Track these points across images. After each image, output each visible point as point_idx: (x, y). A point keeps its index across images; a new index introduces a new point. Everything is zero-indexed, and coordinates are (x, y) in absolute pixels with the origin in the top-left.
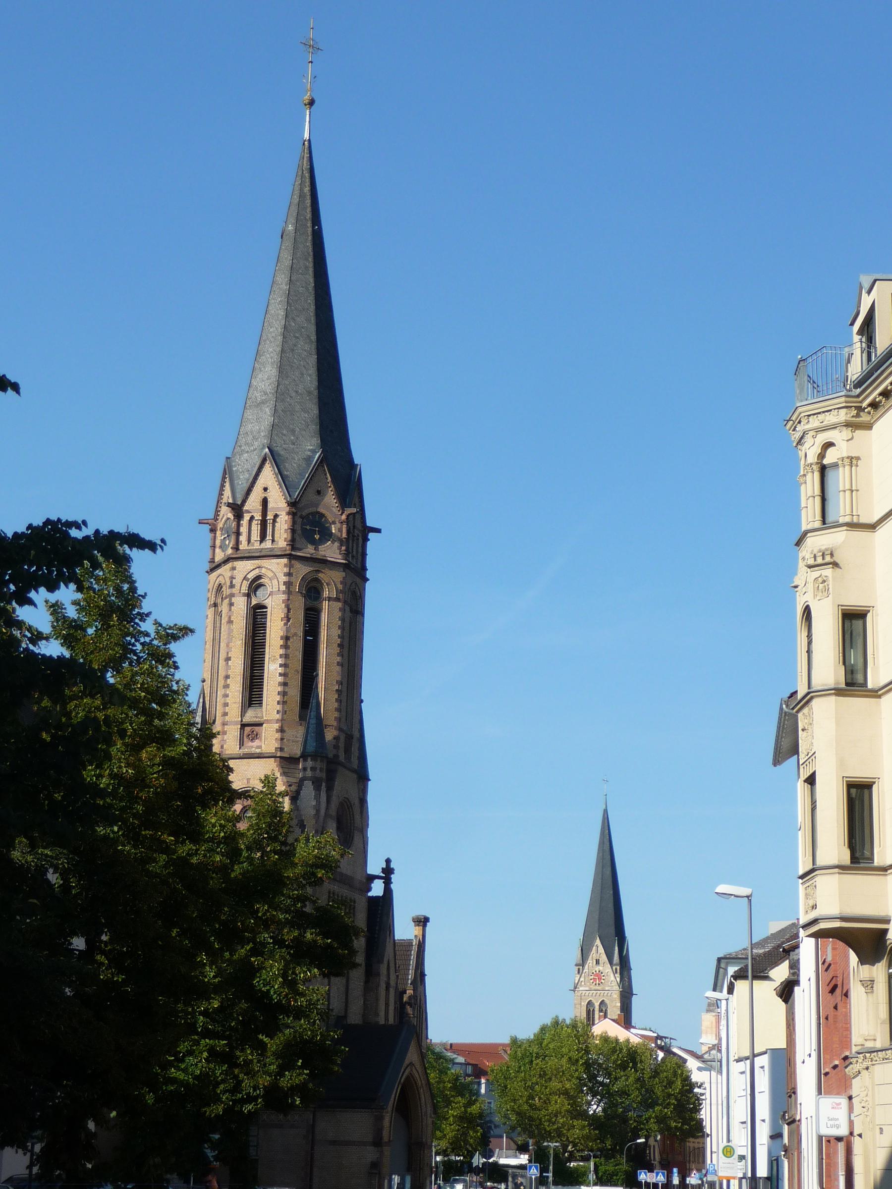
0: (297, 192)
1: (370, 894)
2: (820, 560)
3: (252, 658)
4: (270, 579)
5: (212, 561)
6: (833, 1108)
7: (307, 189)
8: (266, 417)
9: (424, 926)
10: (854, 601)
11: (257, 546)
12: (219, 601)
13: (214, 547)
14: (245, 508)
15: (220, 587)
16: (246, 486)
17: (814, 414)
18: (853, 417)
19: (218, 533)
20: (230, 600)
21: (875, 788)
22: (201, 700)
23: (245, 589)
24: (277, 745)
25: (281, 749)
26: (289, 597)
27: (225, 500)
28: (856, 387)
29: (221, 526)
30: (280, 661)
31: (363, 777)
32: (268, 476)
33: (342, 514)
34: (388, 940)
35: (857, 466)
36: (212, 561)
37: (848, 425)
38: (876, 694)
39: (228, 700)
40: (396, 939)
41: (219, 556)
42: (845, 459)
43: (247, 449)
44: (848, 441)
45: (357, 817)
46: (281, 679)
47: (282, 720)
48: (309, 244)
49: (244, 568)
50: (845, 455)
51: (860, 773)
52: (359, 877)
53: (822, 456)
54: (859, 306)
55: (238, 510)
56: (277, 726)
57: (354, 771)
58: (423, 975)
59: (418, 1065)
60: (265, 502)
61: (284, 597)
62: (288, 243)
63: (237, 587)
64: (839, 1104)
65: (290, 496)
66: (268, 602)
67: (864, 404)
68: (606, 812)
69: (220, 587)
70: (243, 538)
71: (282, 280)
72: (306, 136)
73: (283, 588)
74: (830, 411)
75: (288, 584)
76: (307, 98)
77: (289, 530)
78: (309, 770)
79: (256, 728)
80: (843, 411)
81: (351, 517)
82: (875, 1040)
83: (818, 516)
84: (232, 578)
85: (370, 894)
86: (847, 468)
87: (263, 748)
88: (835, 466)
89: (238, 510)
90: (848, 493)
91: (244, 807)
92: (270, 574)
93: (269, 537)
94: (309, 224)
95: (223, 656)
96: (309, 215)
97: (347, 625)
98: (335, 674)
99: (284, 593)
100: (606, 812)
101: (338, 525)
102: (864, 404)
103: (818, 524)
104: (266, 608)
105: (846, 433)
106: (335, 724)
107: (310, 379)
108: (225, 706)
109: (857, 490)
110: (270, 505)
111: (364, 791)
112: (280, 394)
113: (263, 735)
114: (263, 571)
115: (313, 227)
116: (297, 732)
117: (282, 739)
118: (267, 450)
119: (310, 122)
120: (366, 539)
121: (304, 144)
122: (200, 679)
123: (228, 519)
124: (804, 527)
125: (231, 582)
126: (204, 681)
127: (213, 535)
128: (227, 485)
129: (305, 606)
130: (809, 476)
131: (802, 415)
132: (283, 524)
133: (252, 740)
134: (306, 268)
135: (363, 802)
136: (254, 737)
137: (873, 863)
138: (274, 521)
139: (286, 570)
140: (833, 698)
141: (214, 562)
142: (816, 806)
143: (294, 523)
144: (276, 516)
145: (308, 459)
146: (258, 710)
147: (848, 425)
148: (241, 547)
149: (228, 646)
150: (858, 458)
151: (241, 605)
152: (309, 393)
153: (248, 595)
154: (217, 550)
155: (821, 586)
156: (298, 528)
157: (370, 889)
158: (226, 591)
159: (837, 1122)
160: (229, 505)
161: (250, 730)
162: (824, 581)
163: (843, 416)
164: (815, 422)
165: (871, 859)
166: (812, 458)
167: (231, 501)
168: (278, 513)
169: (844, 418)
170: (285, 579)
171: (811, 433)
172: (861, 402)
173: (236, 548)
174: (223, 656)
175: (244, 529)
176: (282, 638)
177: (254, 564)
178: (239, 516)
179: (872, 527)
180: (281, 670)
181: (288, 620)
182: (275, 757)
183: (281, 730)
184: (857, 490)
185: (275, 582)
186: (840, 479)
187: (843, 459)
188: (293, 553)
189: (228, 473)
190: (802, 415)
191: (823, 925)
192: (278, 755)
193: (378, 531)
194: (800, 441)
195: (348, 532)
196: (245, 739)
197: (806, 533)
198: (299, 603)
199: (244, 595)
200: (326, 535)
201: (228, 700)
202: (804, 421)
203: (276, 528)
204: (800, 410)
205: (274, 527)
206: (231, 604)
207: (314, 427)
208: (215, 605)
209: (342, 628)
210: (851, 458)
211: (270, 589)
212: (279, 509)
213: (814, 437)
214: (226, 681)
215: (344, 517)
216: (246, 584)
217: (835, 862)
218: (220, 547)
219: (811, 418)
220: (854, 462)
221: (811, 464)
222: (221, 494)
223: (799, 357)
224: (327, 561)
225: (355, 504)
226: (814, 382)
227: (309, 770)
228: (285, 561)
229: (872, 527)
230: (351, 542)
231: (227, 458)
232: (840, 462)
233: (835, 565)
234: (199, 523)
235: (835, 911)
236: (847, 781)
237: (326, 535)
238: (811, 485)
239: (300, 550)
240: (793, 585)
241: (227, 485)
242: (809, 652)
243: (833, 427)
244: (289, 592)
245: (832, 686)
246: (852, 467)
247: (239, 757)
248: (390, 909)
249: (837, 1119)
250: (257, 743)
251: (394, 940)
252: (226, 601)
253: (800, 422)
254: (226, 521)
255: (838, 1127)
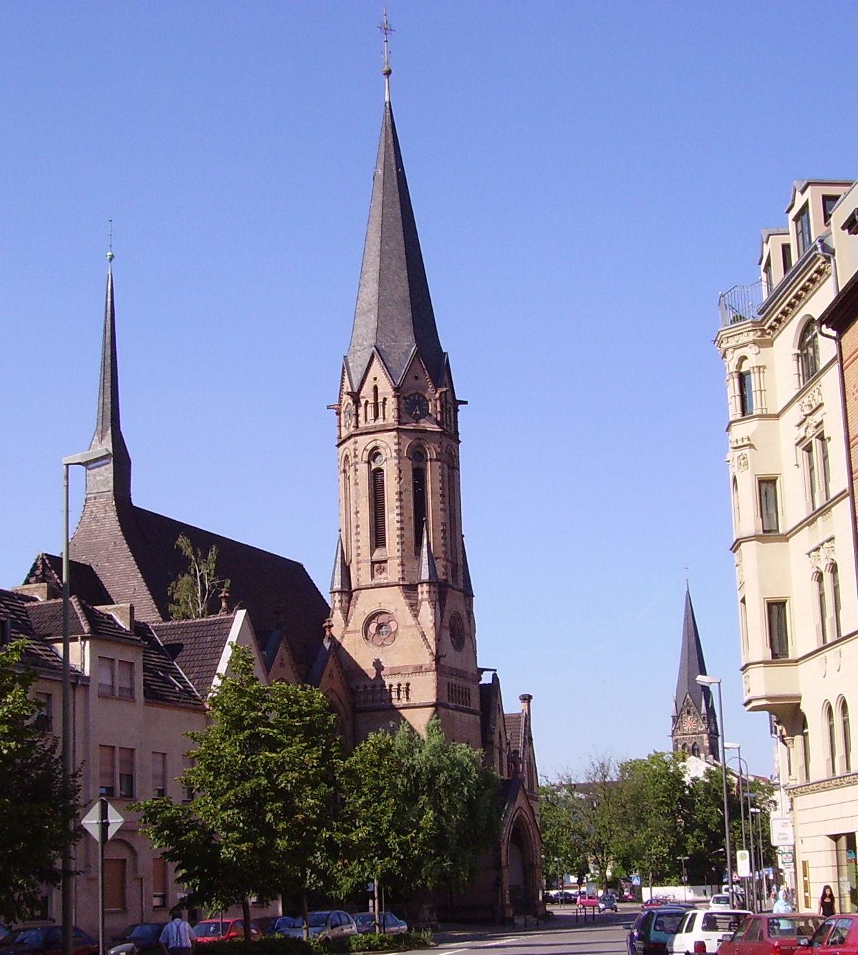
0: (383, 145)
1: (481, 683)
2: (740, 444)
3: (376, 508)
4: (384, 449)
5: (340, 437)
6: (782, 826)
7: (390, 141)
8: (372, 321)
9: (529, 702)
10: (767, 471)
11: (372, 423)
12: (347, 467)
13: (340, 426)
14: (362, 395)
15: (347, 457)
16: (360, 377)
17: (732, 336)
18: (759, 337)
19: (342, 415)
20: (355, 467)
21: (787, 604)
22: (340, 546)
23: (365, 458)
24: (400, 576)
25: (403, 579)
26: (399, 461)
27: (345, 390)
28: (759, 314)
29: (344, 409)
30: (398, 511)
31: (468, 594)
32: (377, 369)
33: (435, 394)
34: (498, 716)
35: (764, 372)
36: (340, 437)
37: (755, 342)
38: (785, 538)
39: (360, 544)
40: (505, 713)
41: (345, 434)
42: (755, 368)
43: (359, 348)
44: (756, 354)
45: (466, 626)
46: (398, 525)
47: (402, 556)
48: (395, 183)
49: (365, 442)
50: (755, 365)
51: (776, 595)
52: (471, 670)
53: (739, 366)
54: (762, 252)
55: (356, 397)
56: (398, 561)
57: (460, 590)
58: (531, 739)
59: (525, 808)
60: (376, 388)
61: (396, 461)
62: (379, 184)
63: (360, 457)
64: (786, 823)
65: (394, 383)
66: (384, 467)
67: (766, 327)
68: (688, 592)
69: (347, 457)
70: (361, 419)
71: (377, 213)
72: (387, 99)
73: (394, 454)
74: (742, 333)
75: (399, 451)
76: (386, 68)
77: (396, 410)
78: (425, 593)
79: (383, 565)
80: (752, 333)
81: (443, 395)
82: (796, 780)
83: (739, 411)
84: (355, 450)
85: (481, 683)
86: (757, 374)
87: (389, 579)
88: (748, 373)
89: (356, 397)
90: (758, 392)
91: (379, 625)
92: (384, 445)
93: (381, 416)
94: (394, 168)
95: (353, 510)
96: (393, 161)
97: (446, 479)
98: (439, 517)
99: (395, 458)
100: (688, 592)
101: (433, 401)
102: (766, 327)
103: (739, 416)
104: (382, 471)
105: (755, 349)
106: (443, 556)
107: (402, 289)
108: (357, 549)
109: (765, 390)
110: (379, 391)
111: (470, 605)
112: (382, 303)
113: (388, 568)
114: (378, 442)
115: (397, 169)
116: (414, 565)
117: (403, 571)
118: (374, 348)
119: (389, 88)
120: (456, 410)
121: (385, 106)
122: (338, 529)
123: (349, 404)
124: (732, 419)
125: (355, 453)
126: (340, 531)
127: (338, 417)
128: (346, 377)
129: (413, 466)
130: (731, 380)
131: (723, 337)
132: (391, 404)
133: (381, 573)
134: (394, 202)
135: (470, 613)
136: (382, 570)
137: (788, 657)
138: (384, 403)
139: (396, 440)
140: (754, 543)
141: (341, 438)
142: (838, 585)
143: (399, 403)
144: (385, 399)
145: (406, 353)
146: (383, 549)
147: (755, 342)
148: (360, 425)
149: (356, 502)
150: (764, 367)
151: (363, 470)
152: (404, 301)
153: (369, 463)
154: (343, 428)
155: (742, 462)
156: (402, 406)
157: (480, 679)
158: (352, 460)
159: (785, 836)
160: (348, 393)
161: (378, 565)
162: (744, 458)
163: (752, 336)
164: (732, 342)
165: (787, 655)
166: (733, 368)
167: (350, 390)
168: (386, 397)
169: (752, 338)
170: (396, 447)
171: (731, 350)
172: (764, 326)
173: (357, 427)
174: (353, 510)
175: (361, 411)
176: (396, 493)
177: (371, 438)
178: (357, 402)
179: (777, 416)
180: (398, 518)
181: (401, 479)
182: (398, 585)
183: (402, 564)
184: (765, 390)
185: (388, 450)
186: (754, 381)
187: (753, 368)
188: (400, 427)
189: (346, 369)
190: (723, 337)
191: (754, 704)
192: (401, 583)
193: (466, 403)
194: (724, 356)
195: (442, 406)
196: (375, 573)
197: (731, 423)
198: (408, 465)
199: (365, 462)
200: (425, 414)
201: (360, 544)
202: (725, 341)
203: (386, 409)
204: (721, 333)
205: (384, 408)
206: (356, 470)
207: (410, 327)
208: (345, 471)
209: (442, 481)
210: (759, 367)
211: (384, 457)
212: (388, 394)
213: (733, 353)
214: (357, 529)
215: (437, 395)
216: (366, 453)
217: (761, 659)
218: (345, 426)
219: (729, 339)
220: (762, 369)
221: (732, 373)
222: (342, 385)
223: (720, 293)
224: (427, 431)
225: (445, 384)
226: (733, 308)
227: (425, 593)
228: (394, 433)
229: (777, 416)
230: (444, 414)
231: (345, 357)
232: (751, 371)
233: (751, 446)
234: (328, 408)
235: (762, 694)
236: (767, 601)
237: (425, 414)
238: (733, 387)
239: (405, 424)
240: (727, 460)
241: (346, 377)
242: (812, 470)
243: (745, 345)
244: (399, 457)
245: (753, 534)
246: (760, 373)
247: (370, 586)
248: (497, 695)
249: (785, 834)
250: (384, 575)
251: (503, 715)
252: (352, 468)
253: (722, 342)
254: (347, 406)
255: (786, 839)
